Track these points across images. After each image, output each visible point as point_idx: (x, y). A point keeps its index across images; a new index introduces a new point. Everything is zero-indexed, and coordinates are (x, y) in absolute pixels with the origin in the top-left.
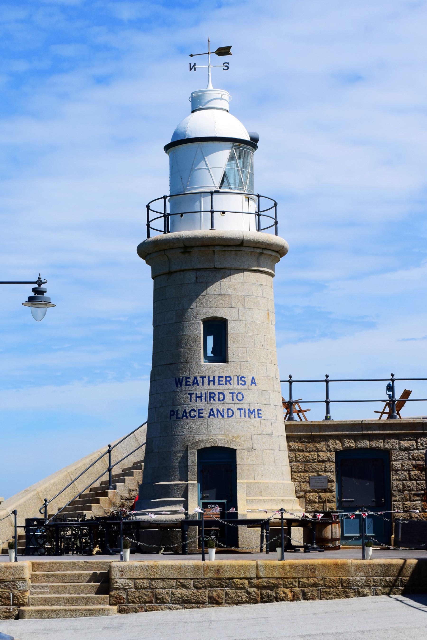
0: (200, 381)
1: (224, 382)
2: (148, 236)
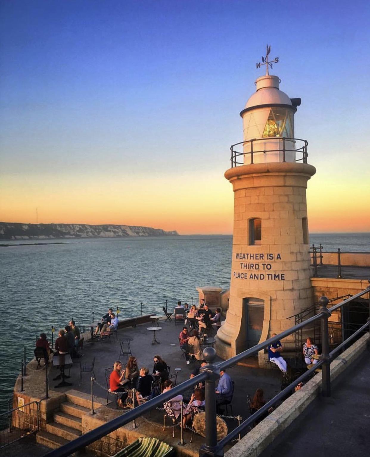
0: (246, 256)
1: (259, 258)
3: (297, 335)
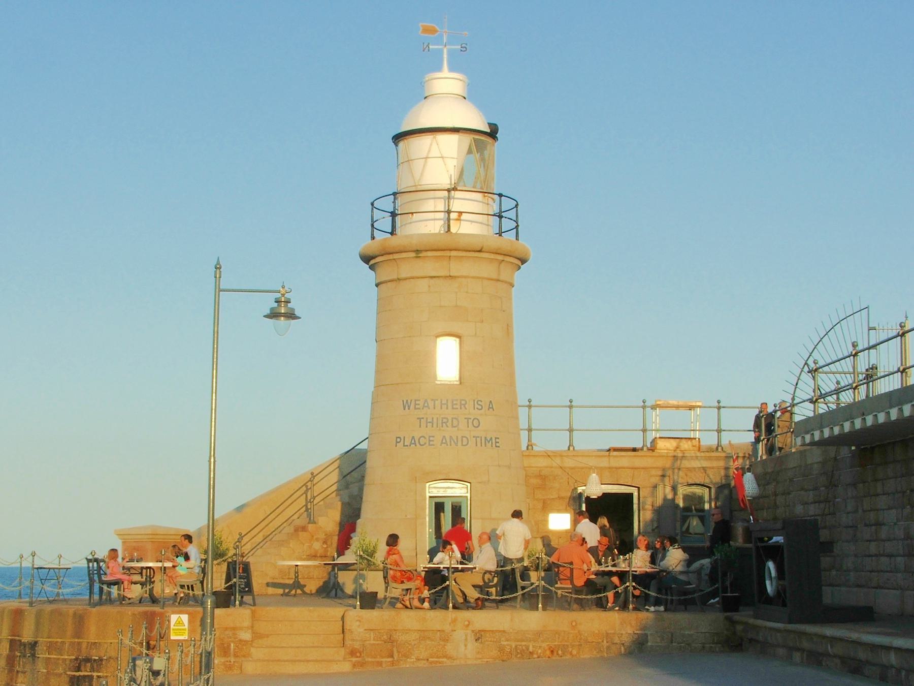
0: (431, 404)
1: (458, 406)
2: (373, 238)
3: (304, 509)
